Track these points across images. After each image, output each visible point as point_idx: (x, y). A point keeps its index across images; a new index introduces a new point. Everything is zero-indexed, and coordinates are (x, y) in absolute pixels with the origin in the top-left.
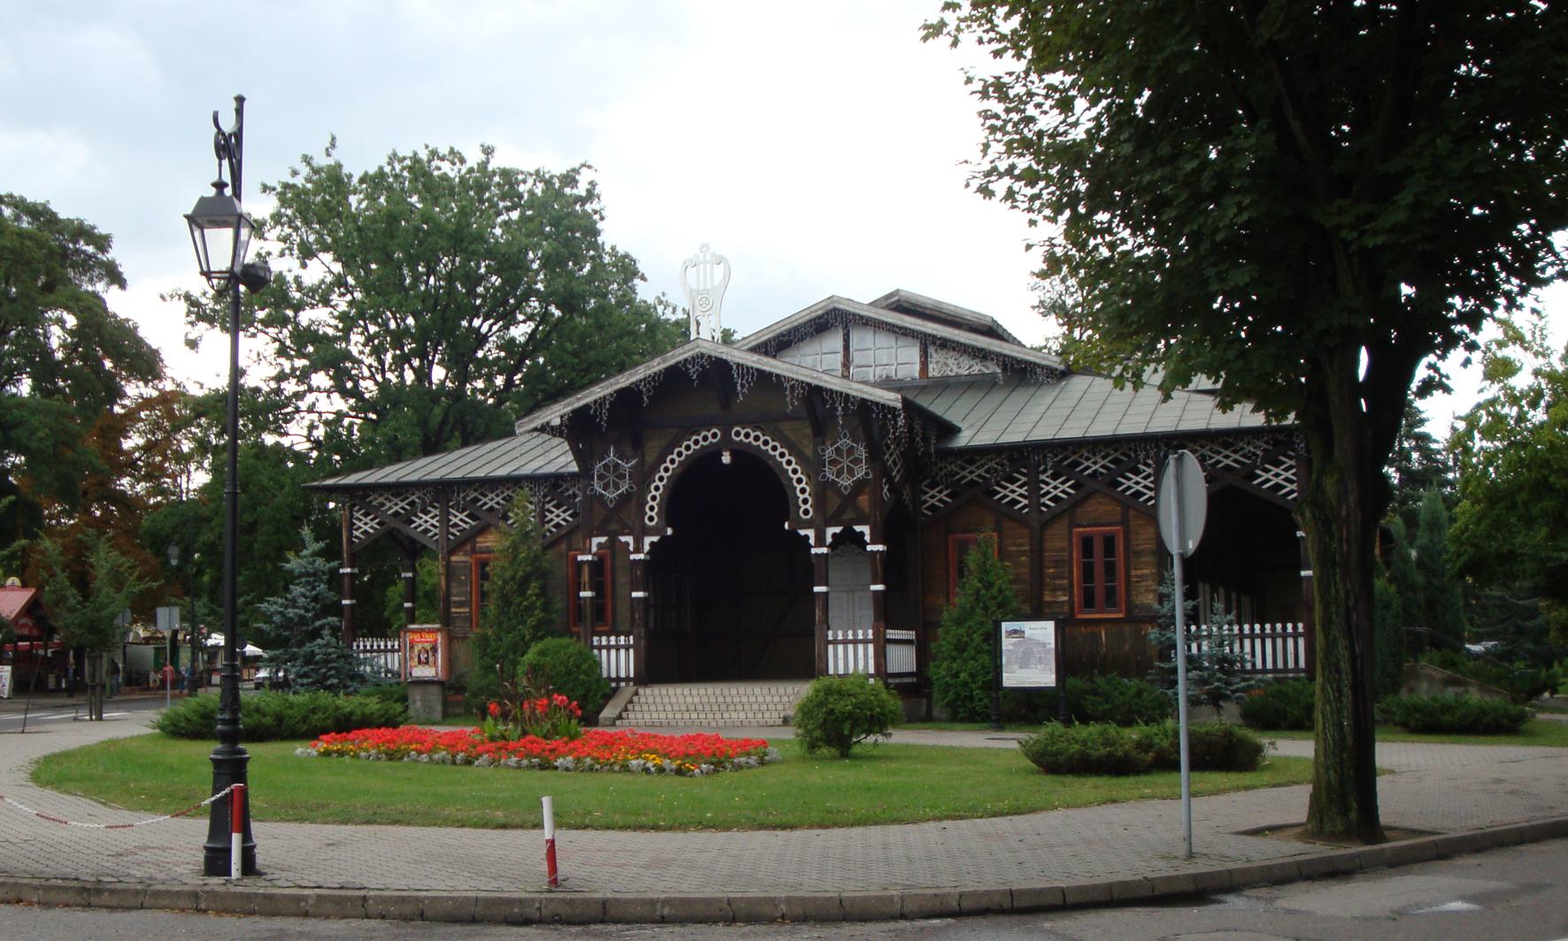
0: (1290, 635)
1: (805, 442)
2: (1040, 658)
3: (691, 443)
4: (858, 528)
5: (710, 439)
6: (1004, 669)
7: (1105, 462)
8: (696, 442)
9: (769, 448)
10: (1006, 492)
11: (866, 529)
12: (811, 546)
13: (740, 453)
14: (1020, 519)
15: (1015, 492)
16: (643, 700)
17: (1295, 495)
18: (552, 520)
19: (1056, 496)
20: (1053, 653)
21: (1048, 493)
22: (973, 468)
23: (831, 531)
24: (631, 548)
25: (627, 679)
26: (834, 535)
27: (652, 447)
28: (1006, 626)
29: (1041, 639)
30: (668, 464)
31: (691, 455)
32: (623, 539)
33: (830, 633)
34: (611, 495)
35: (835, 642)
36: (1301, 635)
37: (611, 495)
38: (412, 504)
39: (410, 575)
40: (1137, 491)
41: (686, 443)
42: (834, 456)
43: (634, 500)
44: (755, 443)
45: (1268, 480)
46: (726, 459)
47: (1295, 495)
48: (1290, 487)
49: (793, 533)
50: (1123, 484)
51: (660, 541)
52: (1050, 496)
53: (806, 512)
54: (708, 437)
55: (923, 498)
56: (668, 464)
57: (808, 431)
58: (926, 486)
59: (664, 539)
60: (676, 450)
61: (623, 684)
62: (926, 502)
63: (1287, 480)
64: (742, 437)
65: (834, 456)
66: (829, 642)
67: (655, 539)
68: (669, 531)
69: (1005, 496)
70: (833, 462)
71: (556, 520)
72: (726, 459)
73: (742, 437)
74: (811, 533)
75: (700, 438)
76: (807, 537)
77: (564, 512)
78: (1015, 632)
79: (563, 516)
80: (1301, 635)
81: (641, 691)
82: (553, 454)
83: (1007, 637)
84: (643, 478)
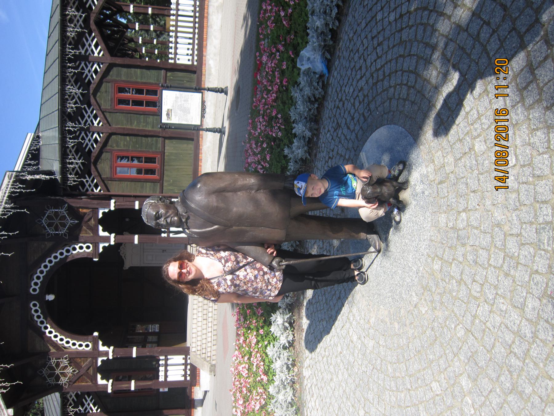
4: (100, 216)
6: (190, 123)
8: (39, 317)
12: (110, 245)
13: (47, 288)
25: (186, 359)
28: (165, 120)
30: (47, 263)
42: (53, 228)
46: (51, 297)
49: (101, 255)
54: (35, 308)
58: (83, 189)
59: (100, 337)
61: (189, 362)
65: (53, 228)
67: (100, 343)
68: (96, 334)
72: (51, 297)
74: (101, 246)
78: (168, 115)
83: (171, 120)
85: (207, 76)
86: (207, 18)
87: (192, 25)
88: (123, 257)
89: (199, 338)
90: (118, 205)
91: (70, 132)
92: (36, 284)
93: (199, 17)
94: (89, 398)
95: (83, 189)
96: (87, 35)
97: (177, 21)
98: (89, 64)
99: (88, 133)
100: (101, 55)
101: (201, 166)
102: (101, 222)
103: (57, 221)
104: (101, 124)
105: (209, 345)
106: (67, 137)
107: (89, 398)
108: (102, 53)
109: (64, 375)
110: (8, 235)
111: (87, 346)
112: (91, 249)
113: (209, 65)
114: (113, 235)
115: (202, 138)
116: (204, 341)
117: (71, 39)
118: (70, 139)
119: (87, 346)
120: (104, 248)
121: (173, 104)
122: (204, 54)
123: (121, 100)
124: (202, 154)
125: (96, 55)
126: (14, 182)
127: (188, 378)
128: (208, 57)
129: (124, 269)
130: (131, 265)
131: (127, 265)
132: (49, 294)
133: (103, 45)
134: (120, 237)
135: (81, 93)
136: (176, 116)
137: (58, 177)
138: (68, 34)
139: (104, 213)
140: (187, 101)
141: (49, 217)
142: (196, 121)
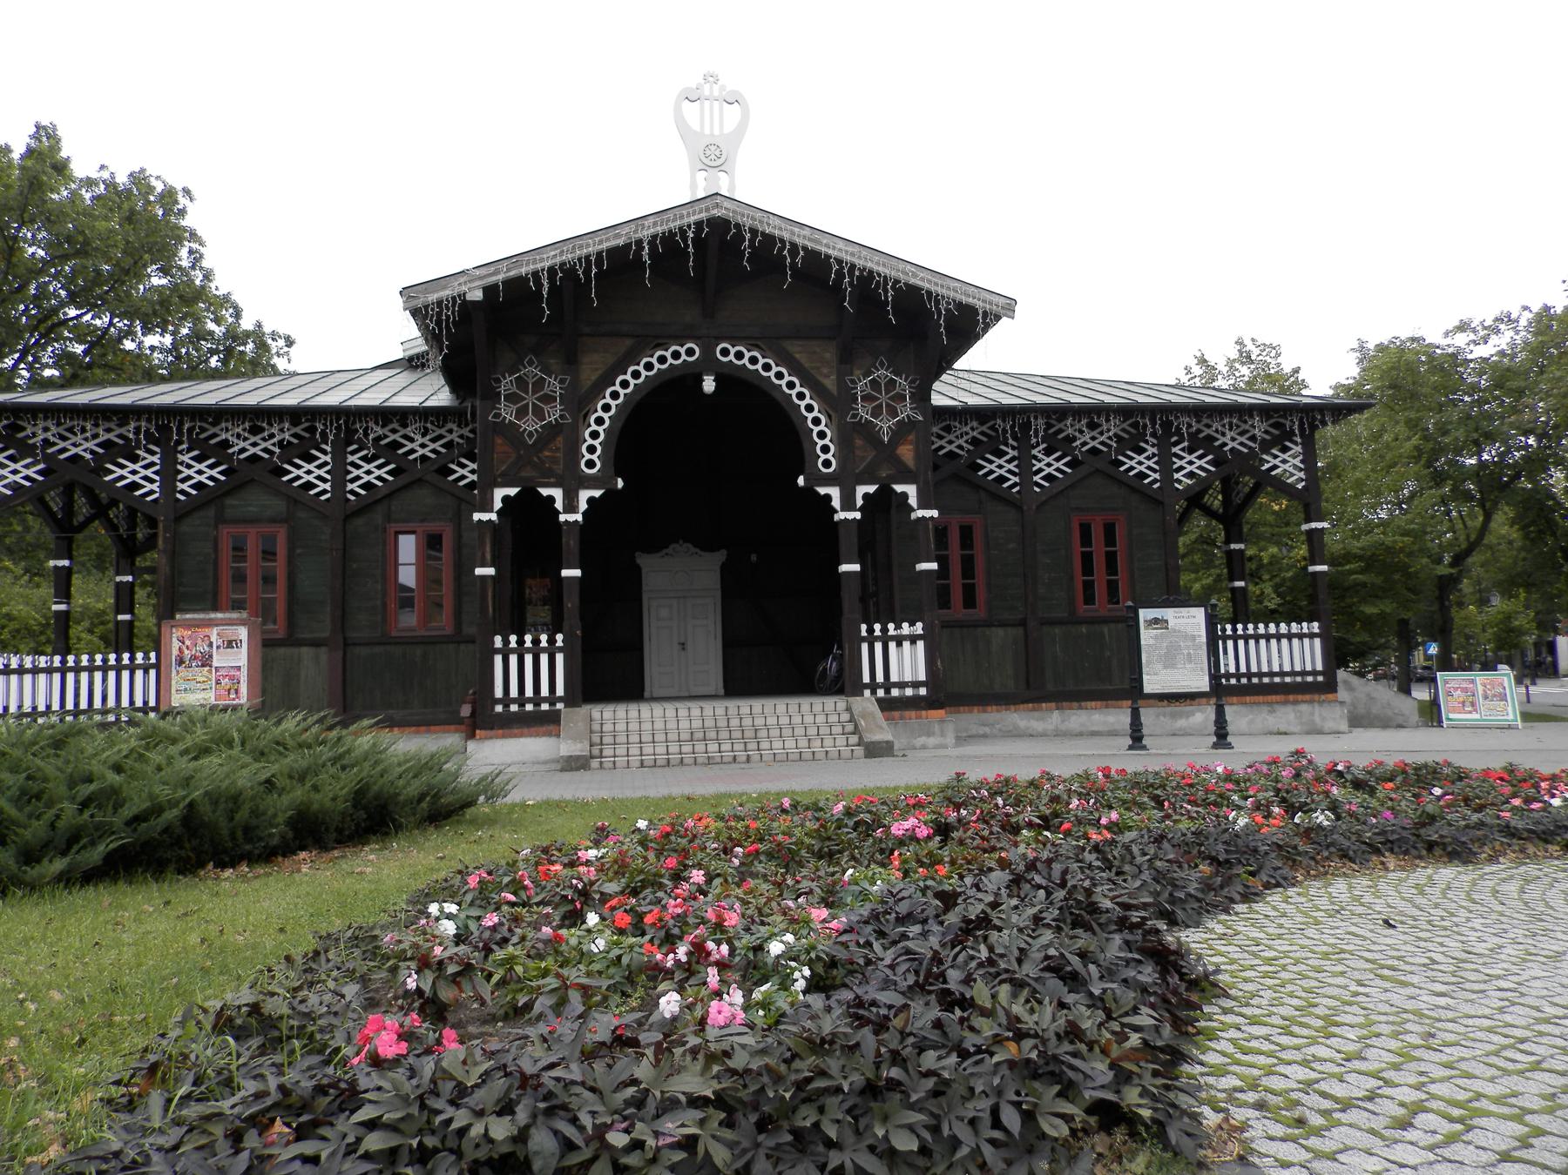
4: (899, 488)
10: (993, 467)
11: (911, 490)
13: (727, 379)
17: (329, 495)
20: (1205, 648)
21: (358, 478)
22: (256, 439)
23: (862, 490)
26: (866, 496)
27: (589, 373)
28: (1145, 614)
29: (1189, 630)
31: (666, 370)
34: (530, 425)
37: (530, 425)
40: (308, 482)
41: (645, 360)
42: (869, 390)
43: (566, 435)
45: (298, 478)
46: (709, 385)
47: (329, 495)
48: (322, 486)
49: (809, 491)
50: (114, 472)
52: (1007, 457)
59: (611, 494)
60: (631, 369)
63: (319, 478)
65: (869, 390)
67: (597, 493)
68: (620, 483)
69: (991, 472)
72: (709, 385)
74: (834, 493)
75: (668, 354)
76: (828, 498)
78: (1156, 621)
83: (1146, 628)
84: (580, 404)
86: (1286, 703)
87: (1243, 669)
88: (665, 551)
92: (739, 355)
93: (1261, 685)
99: (1016, 463)
100: (179, 496)
101: (971, 712)
102: (885, 493)
109: (521, 413)
111: (591, 464)
114: (494, 517)
115: (1034, 709)
123: (971, 533)
124: (998, 711)
129: (637, 554)
130: (644, 571)
131: (645, 561)
136: (1156, 637)
138: (41, 424)
140: (1190, 662)
141: (891, 384)
142: (1151, 684)
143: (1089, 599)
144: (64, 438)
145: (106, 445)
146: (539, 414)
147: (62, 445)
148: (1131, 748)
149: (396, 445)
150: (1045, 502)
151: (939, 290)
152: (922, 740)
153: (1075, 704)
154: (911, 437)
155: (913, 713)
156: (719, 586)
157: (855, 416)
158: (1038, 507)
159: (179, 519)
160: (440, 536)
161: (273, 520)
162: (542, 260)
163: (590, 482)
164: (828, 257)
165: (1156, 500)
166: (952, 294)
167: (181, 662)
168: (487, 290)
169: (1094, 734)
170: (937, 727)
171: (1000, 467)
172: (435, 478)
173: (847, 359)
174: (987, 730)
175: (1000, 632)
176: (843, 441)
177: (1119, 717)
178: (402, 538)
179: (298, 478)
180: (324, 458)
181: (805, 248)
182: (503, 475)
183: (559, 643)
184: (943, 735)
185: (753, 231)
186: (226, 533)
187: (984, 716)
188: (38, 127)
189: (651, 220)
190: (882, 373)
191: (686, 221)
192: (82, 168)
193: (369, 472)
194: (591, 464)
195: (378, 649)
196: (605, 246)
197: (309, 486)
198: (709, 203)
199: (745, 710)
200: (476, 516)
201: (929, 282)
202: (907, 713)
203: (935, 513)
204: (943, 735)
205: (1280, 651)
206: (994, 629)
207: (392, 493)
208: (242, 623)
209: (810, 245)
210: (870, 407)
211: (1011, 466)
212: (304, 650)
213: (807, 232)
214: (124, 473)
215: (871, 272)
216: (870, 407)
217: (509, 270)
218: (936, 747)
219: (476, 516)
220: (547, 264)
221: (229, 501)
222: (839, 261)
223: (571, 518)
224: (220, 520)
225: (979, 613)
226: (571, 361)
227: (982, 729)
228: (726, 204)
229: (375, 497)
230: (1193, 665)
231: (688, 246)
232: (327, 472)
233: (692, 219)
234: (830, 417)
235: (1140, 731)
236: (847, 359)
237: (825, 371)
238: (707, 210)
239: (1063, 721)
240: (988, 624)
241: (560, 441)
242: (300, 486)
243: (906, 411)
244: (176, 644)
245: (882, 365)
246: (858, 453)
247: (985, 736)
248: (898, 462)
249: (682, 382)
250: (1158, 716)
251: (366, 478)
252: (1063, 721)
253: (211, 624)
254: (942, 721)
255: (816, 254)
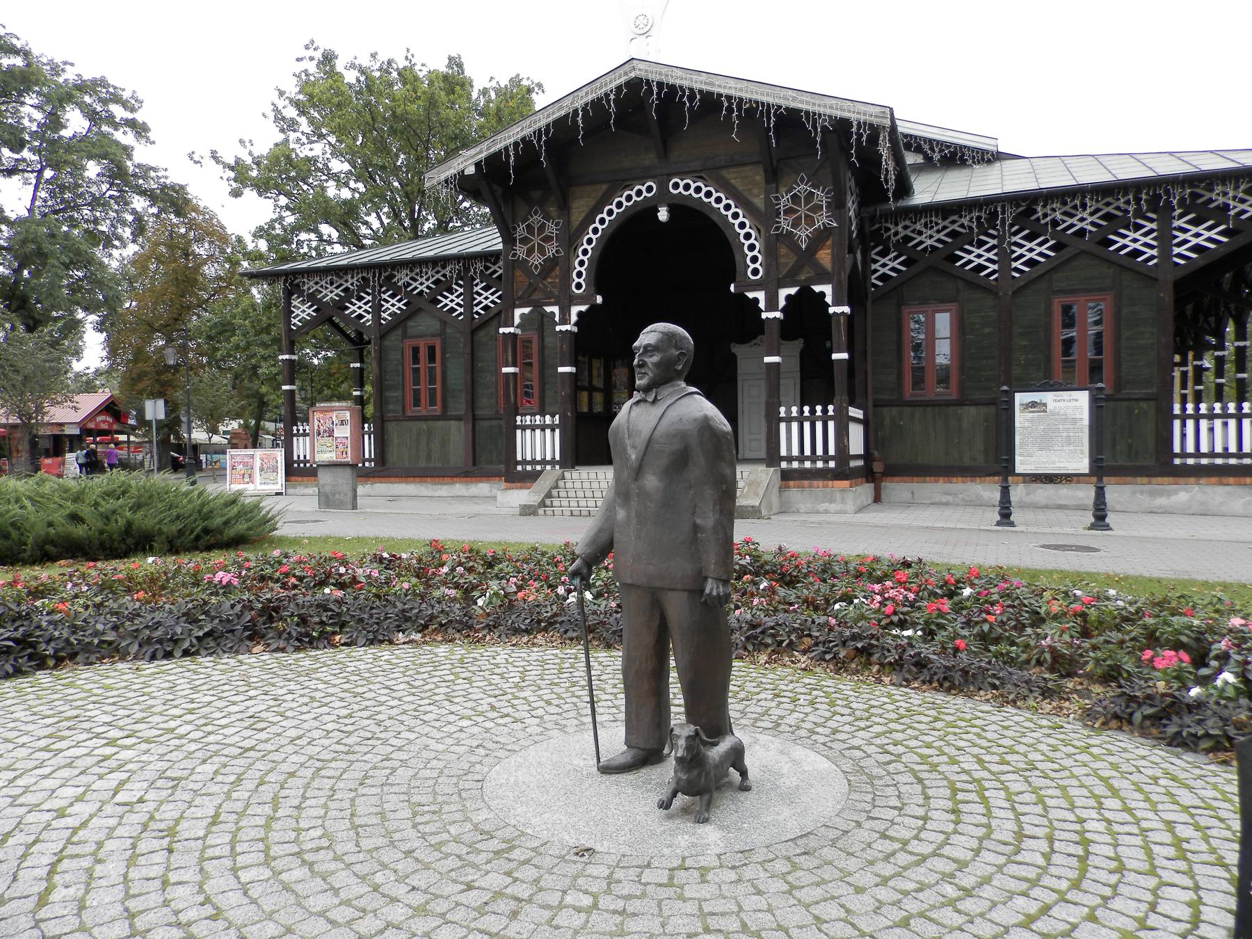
0: (819, 418)
1: (755, 191)
2: (1068, 437)
3: (623, 199)
4: (817, 288)
5: (645, 194)
6: (1017, 451)
7: (1094, 218)
8: (629, 198)
9: (712, 200)
11: (827, 289)
13: (681, 209)
14: (986, 289)
15: (975, 256)
16: (569, 485)
18: (480, 302)
19: (1031, 259)
20: (1087, 431)
21: (1022, 256)
23: (784, 293)
24: (557, 319)
25: (553, 462)
27: (579, 209)
28: (1020, 398)
30: (597, 225)
32: (548, 309)
33: (782, 409)
34: (536, 260)
35: (524, 428)
36: (831, 418)
38: (346, 290)
39: (358, 365)
40: (979, 265)
42: (790, 205)
43: (559, 266)
44: (695, 196)
46: (663, 215)
48: (1150, 252)
49: (741, 297)
50: (1117, 242)
51: (588, 310)
53: (755, 272)
55: (874, 267)
56: (597, 225)
57: (760, 177)
58: (877, 254)
59: (594, 307)
61: (548, 467)
62: (876, 271)
64: (681, 189)
65: (790, 205)
66: (782, 420)
67: (584, 308)
68: (599, 299)
70: (788, 212)
71: (485, 302)
72: (663, 215)
73: (681, 189)
74: (761, 296)
75: (633, 193)
77: (492, 294)
79: (492, 298)
80: (831, 418)
81: (567, 475)
82: (494, 242)
83: (1021, 412)
84: (571, 240)
85: (1147, 487)
89: (586, 485)
90: (839, 321)
91: (994, 215)
94: (900, 264)
95: (877, 254)
96: (1222, 227)
97: (1225, 415)
98: (1014, 252)
101: (937, 482)
102: (805, 292)
103: (803, 210)
104: (1017, 275)
105: (573, 504)
106: (980, 210)
107: (900, 264)
108: (1182, 262)
109: (530, 252)
110: (769, 129)
112: (577, 292)
113: (1176, 492)
116: (580, 494)
117: (1208, 195)
118: (979, 218)
119: (579, 286)
120: (756, 300)
121: (1058, 414)
122: (1203, 481)
125: (1176, 250)
126: (871, 125)
127: (519, 468)
128: (1196, 488)
132: (669, 211)
133: (1202, 263)
134: (776, 329)
135: (422, 291)
136: (1032, 420)
137: (892, 205)
138: (1219, 189)
139: (823, 294)
142: (1022, 464)
143: (417, 403)
144: (415, 280)
145: (437, 282)
146: (542, 250)
147: (1070, 221)
148: (998, 524)
149: (908, 239)
150: (1023, 288)
151: (817, 109)
152: (825, 506)
153: (1192, 480)
154: (829, 242)
155: (821, 483)
156: (798, 368)
157: (778, 228)
158: (1014, 293)
159: (383, 337)
160: (530, 342)
161: (433, 335)
162: (509, 137)
163: (580, 300)
164: (720, 95)
165: (1151, 278)
166: (828, 111)
167: (319, 434)
168: (478, 165)
169: (1060, 507)
170: (838, 495)
171: (979, 256)
172: (1099, 250)
173: (774, 176)
174: (950, 498)
175: (973, 410)
176: (770, 252)
177: (989, 491)
178: (938, 315)
179: (970, 262)
180: (1150, 226)
181: (701, 92)
182: (520, 298)
183: (831, 413)
184: (843, 501)
185: (660, 85)
186: (410, 343)
187: (948, 485)
188: (450, 59)
189: (585, 90)
190: (802, 188)
191: (609, 87)
192: (479, 83)
193: (1031, 250)
194: (579, 286)
195: (494, 423)
196: (550, 119)
197: (1136, 253)
198: (627, 67)
199: (601, 476)
200: (502, 330)
201: (808, 103)
202: (815, 483)
203: (846, 309)
204: (843, 501)
205: (1183, 436)
206: (966, 408)
207: (1054, 268)
208: (347, 409)
209: (705, 88)
210: (791, 219)
211: (990, 255)
212: (452, 422)
213: (703, 77)
214: (1130, 241)
215: (757, 102)
216: (791, 219)
217: (488, 149)
218: (837, 512)
219: (502, 330)
220: (512, 140)
221: (410, 324)
222: (729, 98)
223: (771, 315)
224: (405, 335)
225: (437, 410)
226: (564, 207)
227: (945, 499)
228: (641, 66)
229: (1040, 274)
230: (1072, 448)
231: (610, 106)
232: (1154, 239)
233: (613, 85)
234: (759, 231)
235: (1008, 508)
236: (774, 176)
237: (755, 191)
238: (626, 74)
239: (1028, 494)
240: (960, 403)
241: (557, 271)
242: (1127, 254)
243: (823, 219)
244: (316, 423)
245: (802, 180)
246: (782, 260)
247: (947, 504)
248: (817, 266)
249: (643, 215)
250: (1134, 493)
251: (1029, 255)
252: (1028, 494)
253: (332, 410)
254: (843, 491)
255: (710, 94)
